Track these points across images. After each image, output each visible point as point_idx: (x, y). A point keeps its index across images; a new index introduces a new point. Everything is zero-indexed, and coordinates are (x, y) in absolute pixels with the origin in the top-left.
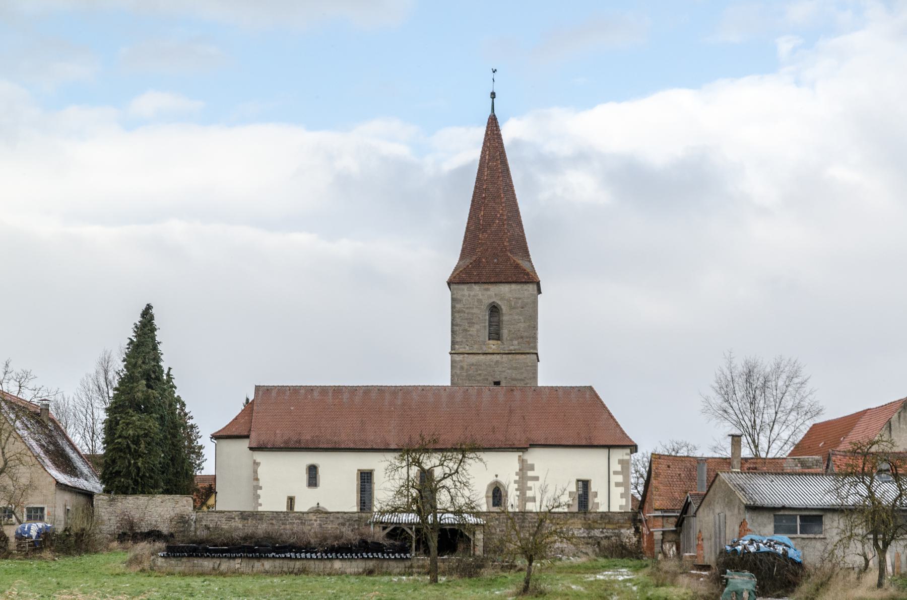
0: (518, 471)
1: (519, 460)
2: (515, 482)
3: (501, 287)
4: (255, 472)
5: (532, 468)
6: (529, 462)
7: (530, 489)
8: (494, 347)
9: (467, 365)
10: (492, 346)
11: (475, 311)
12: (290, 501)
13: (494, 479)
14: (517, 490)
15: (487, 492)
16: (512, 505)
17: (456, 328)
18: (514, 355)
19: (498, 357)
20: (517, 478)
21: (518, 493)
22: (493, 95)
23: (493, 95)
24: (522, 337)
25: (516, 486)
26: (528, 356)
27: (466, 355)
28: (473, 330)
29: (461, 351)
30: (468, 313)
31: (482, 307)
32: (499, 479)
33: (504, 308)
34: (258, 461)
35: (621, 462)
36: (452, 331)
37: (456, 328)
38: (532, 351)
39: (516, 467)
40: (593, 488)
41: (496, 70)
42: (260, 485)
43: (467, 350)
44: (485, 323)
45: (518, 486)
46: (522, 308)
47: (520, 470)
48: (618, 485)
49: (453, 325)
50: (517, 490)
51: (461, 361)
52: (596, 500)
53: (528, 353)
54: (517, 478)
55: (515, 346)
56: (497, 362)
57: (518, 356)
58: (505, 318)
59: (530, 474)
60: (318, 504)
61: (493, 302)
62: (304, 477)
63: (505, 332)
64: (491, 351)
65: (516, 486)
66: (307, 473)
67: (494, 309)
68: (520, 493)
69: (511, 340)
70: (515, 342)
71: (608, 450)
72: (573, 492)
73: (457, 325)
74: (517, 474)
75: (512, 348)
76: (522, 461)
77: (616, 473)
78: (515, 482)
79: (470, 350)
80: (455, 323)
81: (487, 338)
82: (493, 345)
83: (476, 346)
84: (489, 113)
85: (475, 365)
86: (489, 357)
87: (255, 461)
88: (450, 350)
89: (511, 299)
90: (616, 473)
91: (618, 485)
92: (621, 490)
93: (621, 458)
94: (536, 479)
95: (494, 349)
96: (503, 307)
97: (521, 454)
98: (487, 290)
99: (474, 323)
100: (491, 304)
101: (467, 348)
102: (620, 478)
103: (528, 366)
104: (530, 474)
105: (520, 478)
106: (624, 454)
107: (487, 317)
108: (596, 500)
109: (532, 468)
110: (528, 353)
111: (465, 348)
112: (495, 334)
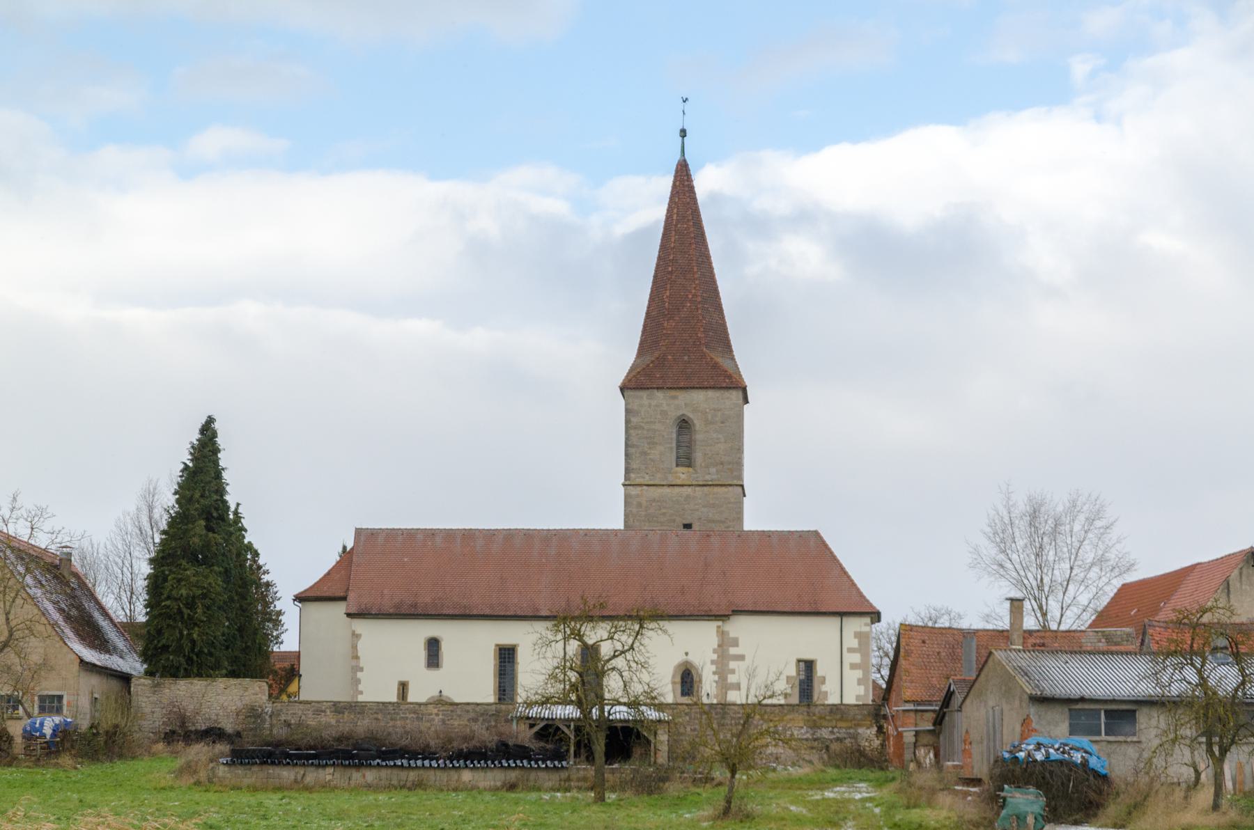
0: (716, 647)
1: (717, 631)
2: (713, 662)
3: (693, 394)
4: (355, 647)
5: (735, 643)
6: (732, 635)
7: (733, 672)
8: (683, 476)
9: (647, 501)
10: (681, 475)
11: (657, 426)
12: (401, 688)
13: (683, 658)
14: (714, 673)
15: (674, 676)
16: (708, 695)
17: (632, 450)
18: (712, 487)
19: (689, 490)
20: (715, 657)
21: (716, 677)
22: (683, 133)
23: (683, 133)
24: (722, 464)
25: (714, 668)
26: (730, 488)
27: (645, 487)
28: (655, 453)
29: (638, 481)
30: (648, 430)
31: (668, 421)
32: (690, 658)
33: (698, 424)
34: (358, 632)
35: (858, 635)
36: (627, 455)
37: (632, 450)
38: (735, 482)
39: (714, 641)
40: (820, 671)
41: (687, 99)
42: (361, 665)
43: (647, 480)
44: (671, 443)
45: (717, 668)
46: (722, 423)
47: (719, 646)
48: (853, 666)
49: (627, 445)
50: (714, 673)
51: (638, 496)
52: (824, 688)
53: (731, 485)
54: (715, 657)
55: (712, 475)
56: (688, 496)
57: (716, 489)
58: (699, 437)
59: (733, 651)
60: (441, 692)
61: (683, 415)
62: (422, 654)
63: (699, 457)
64: (679, 482)
65: (714, 668)
66: (425, 650)
67: (684, 425)
68: (719, 678)
69: (707, 467)
70: (713, 470)
71: (840, 619)
72: (792, 677)
73: (633, 446)
74: (715, 651)
75: (708, 477)
76: (722, 634)
77: (851, 650)
78: (713, 662)
79: (651, 480)
80: (630, 443)
81: (674, 464)
82: (682, 474)
83: (659, 475)
84: (678, 157)
85: (658, 501)
86: (677, 489)
87: (354, 632)
88: (622, 481)
89: (707, 410)
90: (851, 650)
91: (853, 666)
92: (858, 673)
93: (858, 630)
94: (741, 658)
95: (683, 479)
96: (695, 422)
97: (720, 623)
98: (674, 398)
99: (657, 443)
100: (679, 418)
101: (647, 477)
102: (856, 658)
103: (729, 503)
104: (733, 651)
105: (718, 657)
106: (863, 625)
107: (674, 436)
108: (824, 688)
109: (735, 643)
110: (731, 485)
111: (644, 478)
112: (685, 459)
